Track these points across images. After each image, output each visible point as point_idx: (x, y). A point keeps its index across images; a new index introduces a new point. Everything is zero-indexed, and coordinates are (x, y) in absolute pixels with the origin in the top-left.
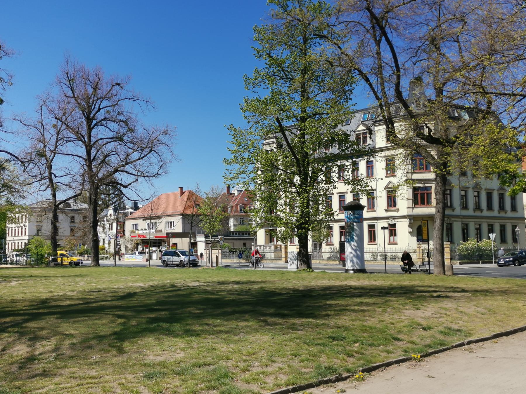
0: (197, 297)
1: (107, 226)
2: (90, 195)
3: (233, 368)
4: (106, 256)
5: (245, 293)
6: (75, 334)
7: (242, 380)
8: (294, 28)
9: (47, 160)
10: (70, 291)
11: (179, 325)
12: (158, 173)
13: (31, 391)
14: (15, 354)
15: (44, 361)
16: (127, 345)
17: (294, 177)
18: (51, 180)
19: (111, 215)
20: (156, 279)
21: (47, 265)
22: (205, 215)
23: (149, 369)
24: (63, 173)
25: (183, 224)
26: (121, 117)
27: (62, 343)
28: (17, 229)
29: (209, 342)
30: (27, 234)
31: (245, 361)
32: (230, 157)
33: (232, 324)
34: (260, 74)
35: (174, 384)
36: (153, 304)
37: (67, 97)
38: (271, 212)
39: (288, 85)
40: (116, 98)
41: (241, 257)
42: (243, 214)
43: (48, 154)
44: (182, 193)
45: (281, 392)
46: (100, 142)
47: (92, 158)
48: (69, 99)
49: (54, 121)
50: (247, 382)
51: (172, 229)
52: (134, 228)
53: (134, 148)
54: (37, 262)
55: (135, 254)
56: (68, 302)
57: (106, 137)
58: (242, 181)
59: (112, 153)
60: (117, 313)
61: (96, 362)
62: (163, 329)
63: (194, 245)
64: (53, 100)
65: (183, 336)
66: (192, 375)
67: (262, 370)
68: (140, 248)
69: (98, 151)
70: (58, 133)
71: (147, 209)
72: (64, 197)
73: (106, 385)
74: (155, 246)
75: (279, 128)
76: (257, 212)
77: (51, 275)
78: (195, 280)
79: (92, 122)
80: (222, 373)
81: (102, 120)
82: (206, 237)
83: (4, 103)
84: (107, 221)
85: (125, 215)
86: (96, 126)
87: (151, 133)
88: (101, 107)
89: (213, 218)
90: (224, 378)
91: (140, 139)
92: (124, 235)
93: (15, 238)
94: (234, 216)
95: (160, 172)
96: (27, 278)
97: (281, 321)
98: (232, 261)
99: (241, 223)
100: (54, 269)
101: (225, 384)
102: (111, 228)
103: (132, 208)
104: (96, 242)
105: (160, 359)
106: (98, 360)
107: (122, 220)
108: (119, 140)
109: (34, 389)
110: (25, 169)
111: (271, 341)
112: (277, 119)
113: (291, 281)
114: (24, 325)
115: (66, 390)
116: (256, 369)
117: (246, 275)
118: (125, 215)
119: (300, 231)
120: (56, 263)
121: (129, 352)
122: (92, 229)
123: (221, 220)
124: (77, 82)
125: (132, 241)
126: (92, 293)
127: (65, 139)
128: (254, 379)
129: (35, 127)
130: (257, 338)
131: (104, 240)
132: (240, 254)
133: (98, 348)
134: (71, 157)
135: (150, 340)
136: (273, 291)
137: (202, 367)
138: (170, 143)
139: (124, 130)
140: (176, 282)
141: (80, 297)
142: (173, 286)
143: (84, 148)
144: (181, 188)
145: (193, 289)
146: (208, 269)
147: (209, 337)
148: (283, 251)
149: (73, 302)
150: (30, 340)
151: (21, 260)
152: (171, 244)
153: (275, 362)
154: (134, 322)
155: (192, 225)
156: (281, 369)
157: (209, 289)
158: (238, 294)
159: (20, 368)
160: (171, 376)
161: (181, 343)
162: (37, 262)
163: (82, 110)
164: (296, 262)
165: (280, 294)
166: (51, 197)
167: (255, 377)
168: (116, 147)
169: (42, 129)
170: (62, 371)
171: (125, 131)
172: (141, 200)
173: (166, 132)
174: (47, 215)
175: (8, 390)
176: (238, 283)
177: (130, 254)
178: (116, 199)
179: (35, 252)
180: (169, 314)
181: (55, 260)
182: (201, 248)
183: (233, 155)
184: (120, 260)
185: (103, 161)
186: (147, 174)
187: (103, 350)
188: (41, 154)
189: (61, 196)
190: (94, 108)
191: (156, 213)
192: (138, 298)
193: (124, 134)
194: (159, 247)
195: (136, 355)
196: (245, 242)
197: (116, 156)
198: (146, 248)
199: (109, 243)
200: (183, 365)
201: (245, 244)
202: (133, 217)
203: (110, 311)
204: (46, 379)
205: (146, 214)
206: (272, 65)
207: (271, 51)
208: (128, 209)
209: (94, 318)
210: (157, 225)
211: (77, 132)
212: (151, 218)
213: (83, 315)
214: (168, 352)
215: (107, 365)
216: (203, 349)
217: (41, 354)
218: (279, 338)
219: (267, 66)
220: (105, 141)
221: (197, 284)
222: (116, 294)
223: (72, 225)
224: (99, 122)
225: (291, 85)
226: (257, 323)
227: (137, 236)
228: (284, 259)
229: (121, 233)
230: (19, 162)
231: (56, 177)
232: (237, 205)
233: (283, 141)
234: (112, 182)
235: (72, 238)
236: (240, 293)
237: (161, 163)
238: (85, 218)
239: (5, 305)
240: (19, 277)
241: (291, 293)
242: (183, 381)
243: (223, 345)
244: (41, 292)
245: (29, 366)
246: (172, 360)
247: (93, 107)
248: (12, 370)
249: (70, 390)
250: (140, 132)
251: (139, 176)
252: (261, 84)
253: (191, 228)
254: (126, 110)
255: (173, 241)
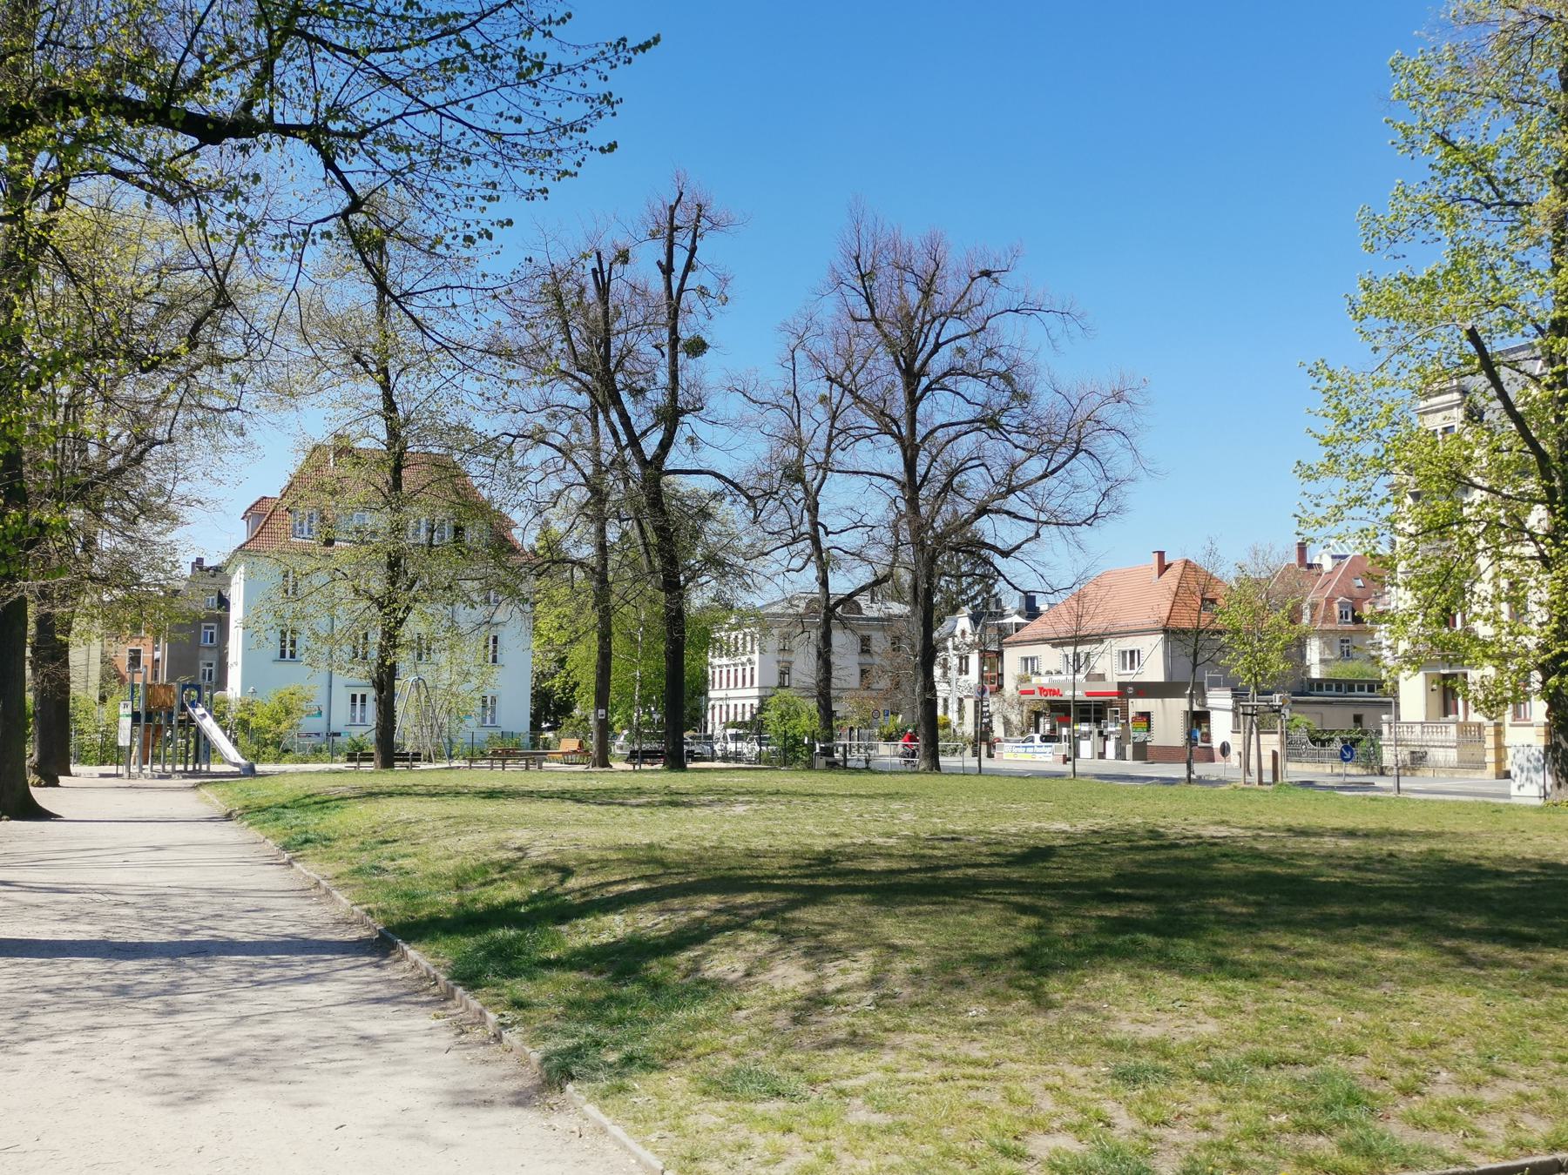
0: (1230, 869)
1: (954, 662)
2: (915, 580)
3: (1370, 1080)
4: (953, 745)
5: (1378, 866)
6: (917, 946)
7: (1402, 1117)
8: (1527, 46)
9: (806, 490)
10: (881, 835)
11: (1191, 943)
12: (1096, 513)
13: (828, 1081)
14: (778, 986)
15: (849, 1008)
16: (1054, 987)
17: (1529, 510)
18: (816, 541)
19: (963, 632)
20: (1103, 812)
21: (810, 766)
22: (1238, 631)
23: (1124, 1055)
24: (844, 523)
25: (1166, 653)
26: (994, 361)
27: (887, 967)
28: (732, 669)
29: (1288, 997)
30: (756, 684)
31: (1406, 1064)
32: (1318, 456)
33: (1354, 954)
34: (1413, 201)
35: (1199, 1105)
36: (1106, 882)
37: (855, 320)
38: (1447, 619)
39: (1509, 225)
40: (980, 312)
41: (1348, 756)
42: (1351, 627)
43: (809, 474)
44: (1163, 568)
45: (1533, 1167)
46: (939, 434)
47: (918, 480)
48: (861, 324)
49: (824, 388)
50: (1420, 1125)
51: (1134, 672)
52: (1026, 669)
53: (1029, 447)
54: (785, 757)
55: (1032, 741)
56: (881, 865)
57: (954, 421)
58: (1355, 527)
59: (970, 464)
60: (1013, 899)
61: (981, 1024)
62: (1147, 951)
63: (1199, 719)
64: (820, 332)
65: (1209, 976)
66: (1250, 1085)
67: (1463, 1097)
68: (1045, 726)
69: (934, 460)
70: (834, 418)
71: (1066, 617)
72: (848, 584)
73: (1012, 1085)
74: (1087, 720)
75: (1477, 361)
76: (1403, 622)
77: (826, 791)
78: (1217, 819)
79: (919, 381)
80: (1341, 1086)
81: (945, 375)
82: (1238, 694)
83: (709, 351)
84: (956, 648)
85: (1003, 632)
86: (929, 393)
87: (1075, 402)
88: (941, 341)
89: (1263, 641)
90: (1345, 1106)
91: (1044, 421)
92: (1001, 687)
93: (732, 693)
94: (1322, 634)
95: (1103, 509)
96: (769, 797)
97: (1510, 954)
98: (1320, 770)
99: (1346, 655)
100: (829, 775)
101: (1352, 1124)
102: (963, 670)
103: (1019, 613)
104: (930, 705)
105: (1149, 1033)
106: (982, 1018)
107: (994, 648)
108: (991, 427)
109: (836, 1076)
110: (756, 517)
111: (1482, 1010)
112: (1473, 335)
113: (1525, 835)
114: (788, 915)
115: (915, 1087)
116: (1445, 1088)
117: (1373, 811)
118: (1003, 632)
119: (1553, 680)
120: (830, 759)
121: (1062, 1007)
122: (920, 671)
123: (1287, 647)
124: (882, 280)
125: (1022, 704)
126: (936, 843)
127: (853, 432)
128: (1441, 1119)
129: (779, 406)
130: (1439, 999)
131: (946, 700)
132: (1346, 748)
133: (981, 987)
134: (865, 480)
135: (1117, 978)
136: (1470, 865)
137: (1274, 1067)
138: (1131, 426)
139: (1001, 398)
140: (1163, 824)
141: (910, 852)
142: (1154, 834)
143: (899, 452)
144: (1161, 554)
145: (1215, 844)
146: (1250, 790)
147: (1284, 983)
148: (1490, 742)
149: (895, 865)
150: (809, 953)
151: (745, 751)
152: (1131, 715)
153: (1504, 1076)
154: (1062, 928)
155: (1195, 659)
156: (1527, 1098)
157: (1262, 847)
158: (1357, 868)
159: (796, 1021)
160: (1185, 1082)
161: (1205, 994)
162: (785, 757)
163: (893, 353)
164: (1539, 778)
165: (1498, 875)
166: (816, 588)
167: (1444, 1113)
168: (980, 447)
169: (795, 410)
170: (895, 1038)
171: (1004, 400)
172: (1050, 591)
173: (1118, 397)
174: (806, 634)
175: (776, 1073)
176: (1351, 834)
177: (1018, 742)
178: (977, 588)
179: (781, 730)
180: (1159, 912)
181: (827, 752)
182: (1222, 727)
183: (1325, 451)
184: (990, 756)
185: (947, 487)
186: (1067, 517)
187: (993, 994)
188: (794, 474)
189: (840, 584)
190: (924, 345)
191: (1091, 626)
192: (1063, 863)
193: (1003, 410)
194: (1098, 721)
195: (1084, 1017)
196: (1359, 711)
197: (982, 469)
198: (1061, 726)
199: (961, 709)
200: (1220, 1055)
201: (1358, 719)
202: (1026, 638)
203: (995, 894)
204: (862, 1055)
205: (1063, 628)
206: (1453, 167)
207: (1449, 127)
208: (1010, 616)
209: (958, 908)
210: (1092, 660)
211: (882, 413)
212: (1078, 640)
213: (927, 900)
214: (1169, 1016)
215: (1008, 1033)
216: (1274, 1019)
217: (839, 991)
218: (1511, 1007)
219: (1437, 173)
220: (952, 431)
221: (1223, 831)
222: (1001, 849)
223: (867, 659)
224: (936, 381)
225: (1516, 224)
226: (1434, 955)
227: (1037, 692)
228: (1491, 768)
229: (992, 681)
230: (742, 497)
231: (827, 533)
232: (1330, 601)
233: (1493, 399)
234: (970, 543)
235: (865, 694)
236: (1365, 863)
237: (1104, 486)
238: (896, 640)
239: (733, 864)
240: (749, 793)
241: (1534, 874)
242: (1224, 1100)
243: (1330, 1010)
244: (810, 835)
245: (814, 1018)
246: (1185, 1040)
247: (922, 340)
248: (777, 1024)
249: (923, 1088)
250: (1046, 401)
251: (1046, 523)
252: (1415, 229)
253: (1194, 670)
254: (1006, 342)
255: (1137, 705)
